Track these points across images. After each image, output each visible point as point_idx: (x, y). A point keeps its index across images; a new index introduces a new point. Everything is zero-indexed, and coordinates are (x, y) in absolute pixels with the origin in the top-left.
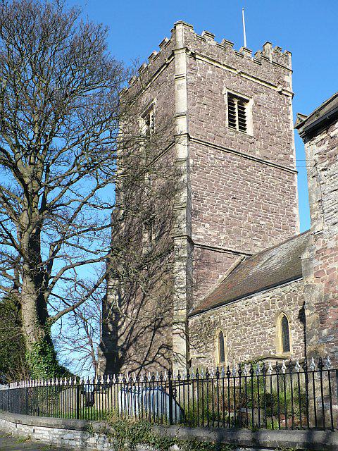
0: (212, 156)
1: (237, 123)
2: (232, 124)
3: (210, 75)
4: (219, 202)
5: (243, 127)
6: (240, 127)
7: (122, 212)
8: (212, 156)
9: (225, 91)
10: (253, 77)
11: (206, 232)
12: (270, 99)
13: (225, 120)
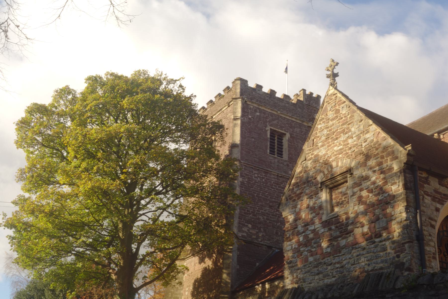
0: (256, 175)
1: (276, 150)
2: (272, 152)
3: (257, 116)
4: (259, 209)
5: (280, 153)
6: (278, 153)
7: (180, 177)
8: (256, 175)
9: (268, 128)
10: (261, 169)
11: (248, 230)
12: (302, 132)
13: (267, 149)
